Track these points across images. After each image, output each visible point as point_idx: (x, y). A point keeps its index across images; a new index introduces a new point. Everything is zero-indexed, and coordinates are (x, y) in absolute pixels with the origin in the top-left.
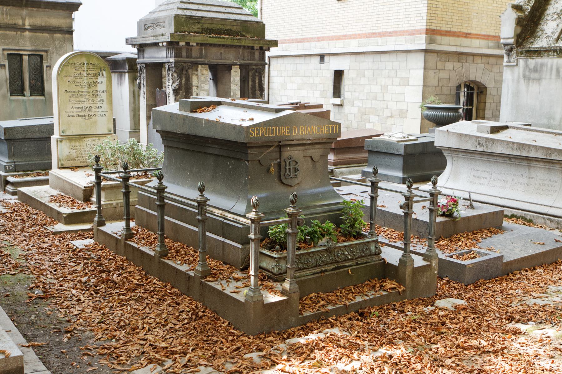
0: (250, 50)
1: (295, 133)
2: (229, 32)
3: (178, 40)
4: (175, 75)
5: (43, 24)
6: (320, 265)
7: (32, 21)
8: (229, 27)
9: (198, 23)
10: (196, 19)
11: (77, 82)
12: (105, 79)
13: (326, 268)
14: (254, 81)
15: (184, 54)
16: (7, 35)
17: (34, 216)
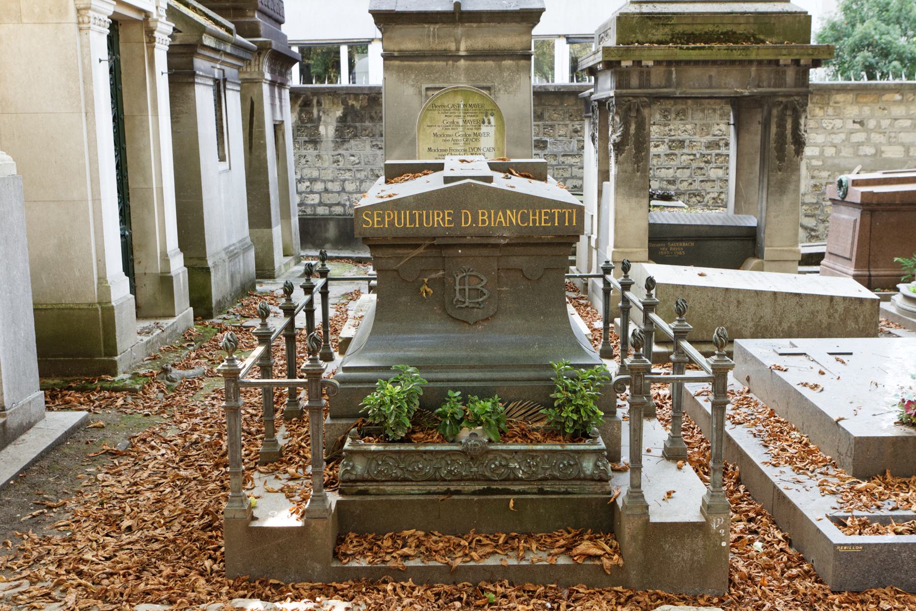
0: (774, 67)
1: (466, 222)
2: (729, 37)
3: (618, 59)
4: (617, 119)
5: (486, 47)
6: (444, 480)
7: (469, 43)
8: (729, 28)
9: (665, 25)
10: (660, 18)
11: (448, 135)
12: (493, 128)
13: (459, 488)
14: (781, 126)
15: (634, 81)
16: (433, 67)
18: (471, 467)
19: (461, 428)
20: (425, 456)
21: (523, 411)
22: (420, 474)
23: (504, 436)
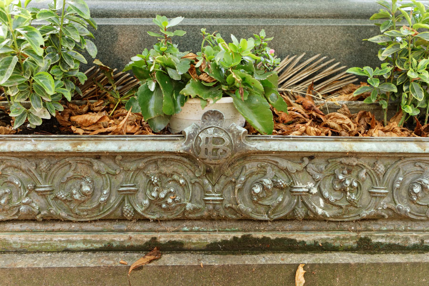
13: (178, 237)
17: (299, 108)
18: (205, 192)
19: (185, 99)
20: (97, 165)
21: (305, 75)
22: (88, 206)
23: (281, 125)
